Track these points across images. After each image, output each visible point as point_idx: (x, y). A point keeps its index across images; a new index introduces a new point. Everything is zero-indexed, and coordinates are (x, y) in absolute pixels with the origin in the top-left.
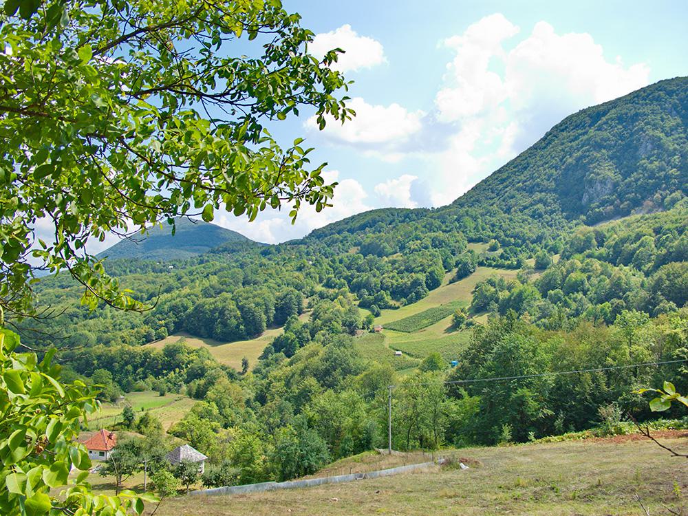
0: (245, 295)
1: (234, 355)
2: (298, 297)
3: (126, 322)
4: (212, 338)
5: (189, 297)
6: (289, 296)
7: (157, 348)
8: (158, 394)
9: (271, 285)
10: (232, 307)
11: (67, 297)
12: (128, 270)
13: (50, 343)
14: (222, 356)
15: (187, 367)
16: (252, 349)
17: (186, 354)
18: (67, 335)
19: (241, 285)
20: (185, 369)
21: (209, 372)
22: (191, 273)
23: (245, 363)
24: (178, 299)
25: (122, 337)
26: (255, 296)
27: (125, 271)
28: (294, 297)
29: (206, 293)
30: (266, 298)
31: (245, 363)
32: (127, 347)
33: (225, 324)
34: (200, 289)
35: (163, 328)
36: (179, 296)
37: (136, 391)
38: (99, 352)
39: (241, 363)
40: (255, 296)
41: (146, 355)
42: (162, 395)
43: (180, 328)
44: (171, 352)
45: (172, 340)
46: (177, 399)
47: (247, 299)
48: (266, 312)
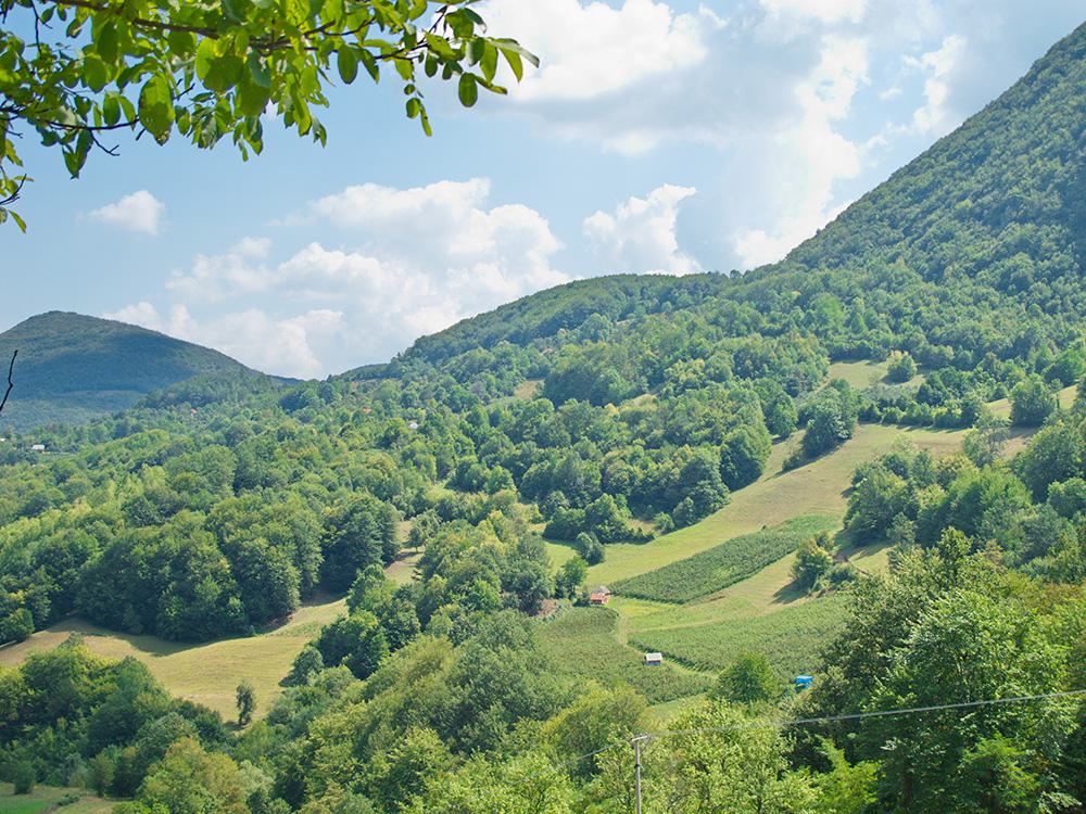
0: (240, 516)
2: (384, 517)
5: (88, 527)
6: (358, 516)
10: (206, 548)
15: (87, 714)
19: (228, 488)
20: (83, 720)
22: (94, 462)
23: (245, 699)
26: (267, 519)
28: (371, 518)
29: (136, 513)
31: (245, 699)
33: (189, 596)
39: (233, 697)
40: (267, 519)
42: (22, 790)
45: (47, 645)
47: (246, 525)
48: (299, 560)
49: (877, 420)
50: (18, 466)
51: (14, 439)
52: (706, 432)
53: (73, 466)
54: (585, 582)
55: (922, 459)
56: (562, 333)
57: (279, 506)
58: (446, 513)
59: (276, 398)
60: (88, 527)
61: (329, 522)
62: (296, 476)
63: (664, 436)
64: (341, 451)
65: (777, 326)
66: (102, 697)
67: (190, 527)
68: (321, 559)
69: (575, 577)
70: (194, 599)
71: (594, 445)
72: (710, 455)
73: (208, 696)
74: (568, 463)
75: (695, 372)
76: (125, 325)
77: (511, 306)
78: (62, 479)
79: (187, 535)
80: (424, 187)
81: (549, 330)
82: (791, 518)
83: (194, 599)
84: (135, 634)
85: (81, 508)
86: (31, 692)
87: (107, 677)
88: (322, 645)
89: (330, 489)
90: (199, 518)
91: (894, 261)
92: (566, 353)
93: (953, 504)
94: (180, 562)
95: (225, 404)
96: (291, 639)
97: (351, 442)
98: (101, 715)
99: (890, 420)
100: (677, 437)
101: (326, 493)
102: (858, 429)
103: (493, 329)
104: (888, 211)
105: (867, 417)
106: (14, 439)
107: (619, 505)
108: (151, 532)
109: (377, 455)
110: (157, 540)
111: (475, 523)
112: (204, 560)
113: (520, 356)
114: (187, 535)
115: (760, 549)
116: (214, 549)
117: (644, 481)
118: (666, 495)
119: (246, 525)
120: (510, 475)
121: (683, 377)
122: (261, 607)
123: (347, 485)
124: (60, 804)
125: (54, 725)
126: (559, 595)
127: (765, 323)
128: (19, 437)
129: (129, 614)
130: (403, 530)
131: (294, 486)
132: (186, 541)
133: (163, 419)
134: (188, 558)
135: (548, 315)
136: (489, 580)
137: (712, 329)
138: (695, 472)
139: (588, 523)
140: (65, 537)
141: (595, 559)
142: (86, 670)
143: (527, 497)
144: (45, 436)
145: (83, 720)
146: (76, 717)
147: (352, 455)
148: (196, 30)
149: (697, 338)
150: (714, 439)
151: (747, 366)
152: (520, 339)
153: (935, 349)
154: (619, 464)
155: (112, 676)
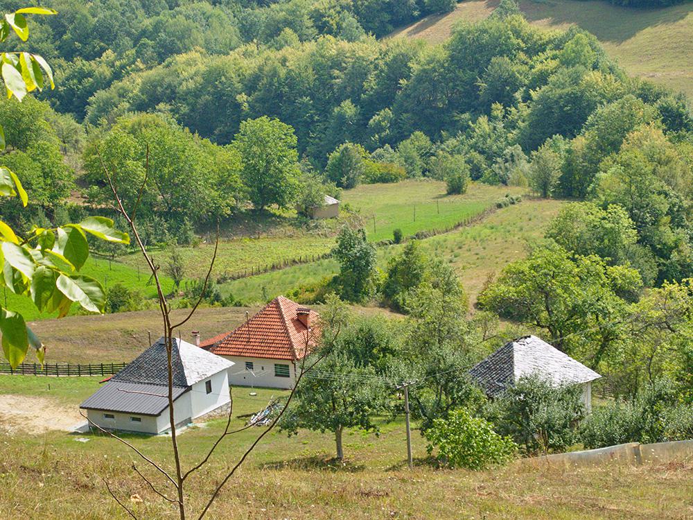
8: (443, 187)
13: (103, 50)
15: (527, 98)
17: (522, 56)
18: (148, 23)
20: (521, 105)
21: (599, 110)
32: (333, 46)
37: (374, 181)
38: (250, 66)
41: (398, 67)
44: (473, 53)
46: (502, 200)
66: (542, 79)
73: (674, 74)
87: (549, 53)
98: (544, 100)
124: (499, 206)
142: (523, 45)
145: (521, 105)
155: (554, 52)
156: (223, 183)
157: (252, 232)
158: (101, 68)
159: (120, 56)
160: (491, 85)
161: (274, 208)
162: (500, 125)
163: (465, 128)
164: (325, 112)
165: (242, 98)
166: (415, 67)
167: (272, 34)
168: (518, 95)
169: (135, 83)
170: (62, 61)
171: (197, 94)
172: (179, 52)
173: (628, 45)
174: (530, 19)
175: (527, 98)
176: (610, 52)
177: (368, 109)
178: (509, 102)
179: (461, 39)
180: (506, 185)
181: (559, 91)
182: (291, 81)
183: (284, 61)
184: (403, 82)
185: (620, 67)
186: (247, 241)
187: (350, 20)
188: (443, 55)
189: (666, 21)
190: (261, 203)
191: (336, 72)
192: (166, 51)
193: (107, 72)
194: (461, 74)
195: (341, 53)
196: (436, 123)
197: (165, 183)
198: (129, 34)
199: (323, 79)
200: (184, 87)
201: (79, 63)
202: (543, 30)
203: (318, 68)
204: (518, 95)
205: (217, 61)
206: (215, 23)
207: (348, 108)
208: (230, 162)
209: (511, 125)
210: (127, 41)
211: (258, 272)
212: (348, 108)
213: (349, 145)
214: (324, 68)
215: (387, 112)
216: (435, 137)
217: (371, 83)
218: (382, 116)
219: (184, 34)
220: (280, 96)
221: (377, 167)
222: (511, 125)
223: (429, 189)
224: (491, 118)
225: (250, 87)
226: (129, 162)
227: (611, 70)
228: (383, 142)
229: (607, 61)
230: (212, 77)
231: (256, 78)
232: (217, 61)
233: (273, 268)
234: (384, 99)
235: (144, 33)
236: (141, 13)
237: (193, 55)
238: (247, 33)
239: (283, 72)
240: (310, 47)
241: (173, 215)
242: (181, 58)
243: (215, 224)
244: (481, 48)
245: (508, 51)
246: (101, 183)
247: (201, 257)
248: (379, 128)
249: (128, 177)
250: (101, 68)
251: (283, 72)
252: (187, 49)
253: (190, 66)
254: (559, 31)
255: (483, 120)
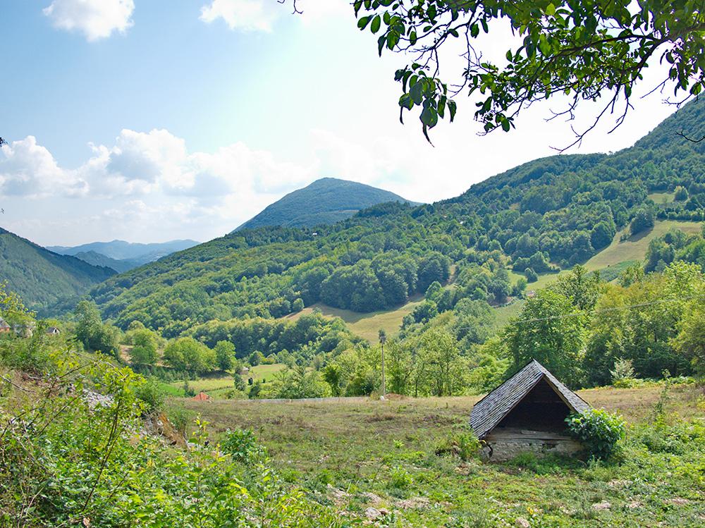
0: (386, 261)
1: (374, 326)
2: (443, 262)
3: (262, 295)
4: (350, 309)
5: (325, 266)
6: (432, 261)
7: (290, 321)
9: (415, 249)
10: (370, 275)
11: (206, 270)
12: (269, 240)
14: (366, 327)
15: (320, 340)
16: (391, 321)
17: (320, 326)
18: (202, 309)
19: (381, 250)
20: (318, 342)
24: (315, 268)
25: (257, 310)
27: (266, 241)
28: (438, 262)
30: (407, 263)
33: (362, 294)
34: (337, 256)
35: (298, 299)
36: (315, 265)
38: (233, 325)
40: (395, 263)
41: (280, 328)
43: (311, 299)
44: (304, 324)
45: (307, 313)
47: (386, 265)
48: (408, 280)
49: (666, 218)
50: (306, 242)
51: (306, 231)
52: (586, 224)
53: (325, 241)
54: (526, 289)
55: (679, 236)
56: (532, 181)
57: (400, 257)
58: (471, 259)
59: (411, 211)
60: (325, 266)
61: (422, 265)
62: (409, 245)
63: (568, 227)
64: (430, 234)
65: (625, 176)
66: (325, 334)
67: (365, 266)
68: (417, 279)
69: (522, 287)
70: (365, 295)
71: (536, 230)
72: (587, 234)
74: (524, 238)
75: (586, 198)
76: (354, 182)
77: (512, 170)
78: (320, 247)
79: (363, 269)
80: (147, 133)
81: (526, 180)
82: (621, 262)
83: (365, 295)
84: (343, 309)
85: (323, 259)
86: (299, 331)
87: (328, 325)
88: (415, 315)
89: (424, 250)
90: (369, 262)
91: (682, 145)
92: (529, 192)
93: (687, 256)
94: (359, 280)
95: (390, 215)
96: (404, 312)
97: (435, 230)
98: (324, 340)
99: (672, 218)
100: (573, 227)
101: (421, 252)
102: (656, 222)
103: (503, 180)
104: (682, 122)
105: (662, 217)
106: (306, 231)
107: (546, 257)
108: (349, 268)
109: (444, 236)
110: (351, 272)
111: (481, 264)
112: (369, 279)
113: (513, 194)
114: (363, 269)
115: (604, 275)
116: (373, 275)
117: (558, 247)
118: (566, 251)
119: (386, 265)
120: (499, 244)
121: (580, 200)
122: (395, 301)
123: (431, 248)
125: (307, 344)
126: (513, 295)
127: (620, 175)
128: (308, 229)
129: (340, 301)
130: (452, 270)
131: (409, 249)
132: (362, 272)
133: (365, 221)
134: (363, 279)
135: (527, 173)
136: (482, 288)
137: (595, 178)
138: (580, 242)
139: (531, 264)
140: (317, 270)
141: (532, 279)
143: (507, 253)
144: (318, 229)
145: (318, 342)
146: (315, 341)
147: (434, 236)
148: (651, 12)
149: (589, 183)
150: (590, 227)
151: (610, 194)
152: (512, 185)
153: (698, 185)
154: (547, 238)
156: (209, 361)
157: (218, 377)
158: (185, 324)
159: (192, 320)
160: (309, 335)
161: (227, 371)
162: (311, 348)
163: (300, 349)
164: (256, 341)
165: (229, 336)
166: (285, 328)
167: (241, 315)
168: (317, 339)
169: (195, 329)
170: (173, 321)
171: (214, 333)
172: (211, 320)
173: (356, 324)
174: (324, 314)
175: (320, 340)
176: (348, 326)
177: (270, 341)
178: (314, 341)
179: (301, 319)
180: (594, 272)
181: (329, 338)
182: (246, 331)
183: (244, 324)
184: (281, 333)
185: (351, 331)
186: (216, 380)
187: (267, 311)
188: (295, 325)
189: (368, 317)
190: (223, 368)
191: (260, 329)
192: (207, 319)
193: (187, 325)
194: (299, 331)
195: (263, 323)
196: (291, 347)
197: (191, 360)
198: (196, 313)
199: (256, 331)
200: (211, 331)
201: (178, 321)
202: (329, 318)
203: (255, 327)
204: (317, 339)
205: (222, 323)
206: (224, 311)
207: (263, 340)
208: (213, 355)
209: (314, 348)
210: (195, 315)
211: (215, 390)
212: (263, 340)
213: (257, 352)
214: (256, 327)
215: (276, 342)
216: (290, 351)
217: (271, 332)
218: (274, 344)
219: (214, 313)
220: (242, 336)
221: (266, 360)
222: (314, 348)
223: (282, 366)
224: (308, 346)
225: (232, 332)
226: (178, 352)
227: (348, 332)
228: (273, 352)
229: (346, 329)
230: (220, 328)
231: (234, 329)
232: (222, 323)
233: (220, 388)
234: (275, 338)
235: (200, 313)
236: (201, 306)
237: (215, 321)
238: (234, 314)
239: (243, 328)
240: (253, 320)
241: (191, 371)
242: (211, 322)
243: (206, 374)
244: (307, 323)
245: (315, 324)
246: (169, 359)
247: (198, 384)
248: (272, 347)
249: (178, 357)
250: (185, 324)
251: (243, 328)
252: (214, 319)
253: (213, 325)
254: (333, 319)
255: (305, 346)
